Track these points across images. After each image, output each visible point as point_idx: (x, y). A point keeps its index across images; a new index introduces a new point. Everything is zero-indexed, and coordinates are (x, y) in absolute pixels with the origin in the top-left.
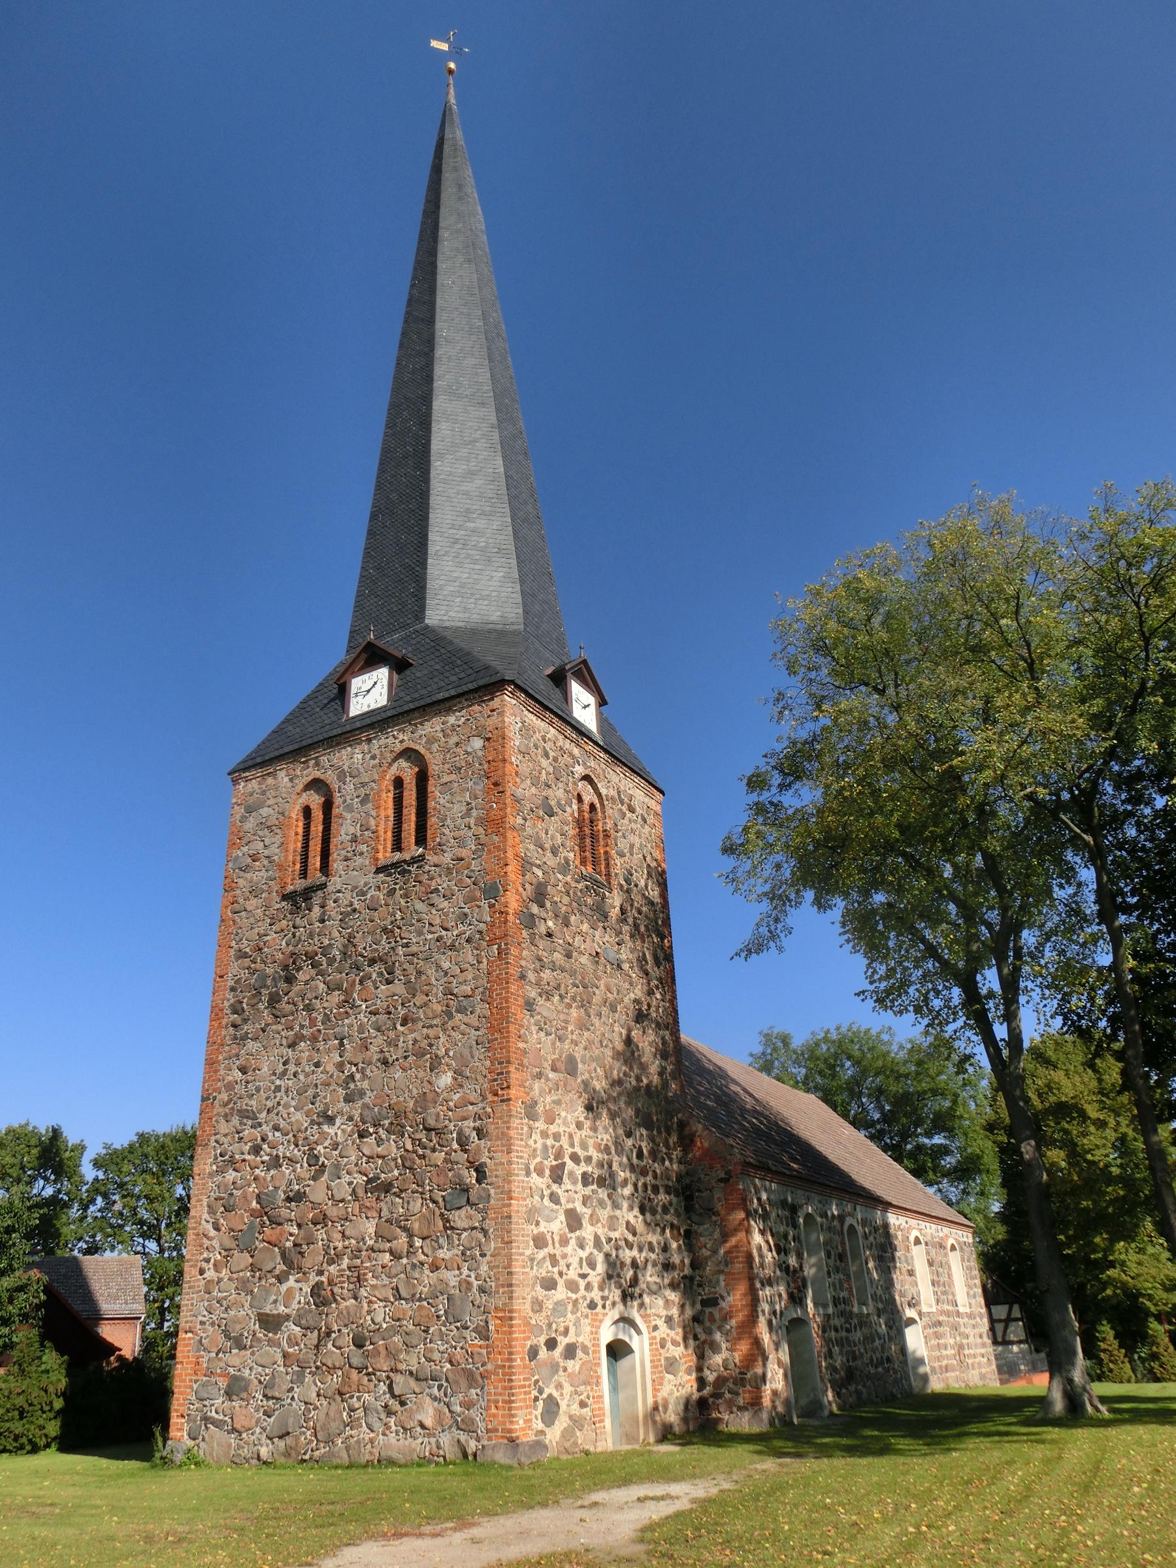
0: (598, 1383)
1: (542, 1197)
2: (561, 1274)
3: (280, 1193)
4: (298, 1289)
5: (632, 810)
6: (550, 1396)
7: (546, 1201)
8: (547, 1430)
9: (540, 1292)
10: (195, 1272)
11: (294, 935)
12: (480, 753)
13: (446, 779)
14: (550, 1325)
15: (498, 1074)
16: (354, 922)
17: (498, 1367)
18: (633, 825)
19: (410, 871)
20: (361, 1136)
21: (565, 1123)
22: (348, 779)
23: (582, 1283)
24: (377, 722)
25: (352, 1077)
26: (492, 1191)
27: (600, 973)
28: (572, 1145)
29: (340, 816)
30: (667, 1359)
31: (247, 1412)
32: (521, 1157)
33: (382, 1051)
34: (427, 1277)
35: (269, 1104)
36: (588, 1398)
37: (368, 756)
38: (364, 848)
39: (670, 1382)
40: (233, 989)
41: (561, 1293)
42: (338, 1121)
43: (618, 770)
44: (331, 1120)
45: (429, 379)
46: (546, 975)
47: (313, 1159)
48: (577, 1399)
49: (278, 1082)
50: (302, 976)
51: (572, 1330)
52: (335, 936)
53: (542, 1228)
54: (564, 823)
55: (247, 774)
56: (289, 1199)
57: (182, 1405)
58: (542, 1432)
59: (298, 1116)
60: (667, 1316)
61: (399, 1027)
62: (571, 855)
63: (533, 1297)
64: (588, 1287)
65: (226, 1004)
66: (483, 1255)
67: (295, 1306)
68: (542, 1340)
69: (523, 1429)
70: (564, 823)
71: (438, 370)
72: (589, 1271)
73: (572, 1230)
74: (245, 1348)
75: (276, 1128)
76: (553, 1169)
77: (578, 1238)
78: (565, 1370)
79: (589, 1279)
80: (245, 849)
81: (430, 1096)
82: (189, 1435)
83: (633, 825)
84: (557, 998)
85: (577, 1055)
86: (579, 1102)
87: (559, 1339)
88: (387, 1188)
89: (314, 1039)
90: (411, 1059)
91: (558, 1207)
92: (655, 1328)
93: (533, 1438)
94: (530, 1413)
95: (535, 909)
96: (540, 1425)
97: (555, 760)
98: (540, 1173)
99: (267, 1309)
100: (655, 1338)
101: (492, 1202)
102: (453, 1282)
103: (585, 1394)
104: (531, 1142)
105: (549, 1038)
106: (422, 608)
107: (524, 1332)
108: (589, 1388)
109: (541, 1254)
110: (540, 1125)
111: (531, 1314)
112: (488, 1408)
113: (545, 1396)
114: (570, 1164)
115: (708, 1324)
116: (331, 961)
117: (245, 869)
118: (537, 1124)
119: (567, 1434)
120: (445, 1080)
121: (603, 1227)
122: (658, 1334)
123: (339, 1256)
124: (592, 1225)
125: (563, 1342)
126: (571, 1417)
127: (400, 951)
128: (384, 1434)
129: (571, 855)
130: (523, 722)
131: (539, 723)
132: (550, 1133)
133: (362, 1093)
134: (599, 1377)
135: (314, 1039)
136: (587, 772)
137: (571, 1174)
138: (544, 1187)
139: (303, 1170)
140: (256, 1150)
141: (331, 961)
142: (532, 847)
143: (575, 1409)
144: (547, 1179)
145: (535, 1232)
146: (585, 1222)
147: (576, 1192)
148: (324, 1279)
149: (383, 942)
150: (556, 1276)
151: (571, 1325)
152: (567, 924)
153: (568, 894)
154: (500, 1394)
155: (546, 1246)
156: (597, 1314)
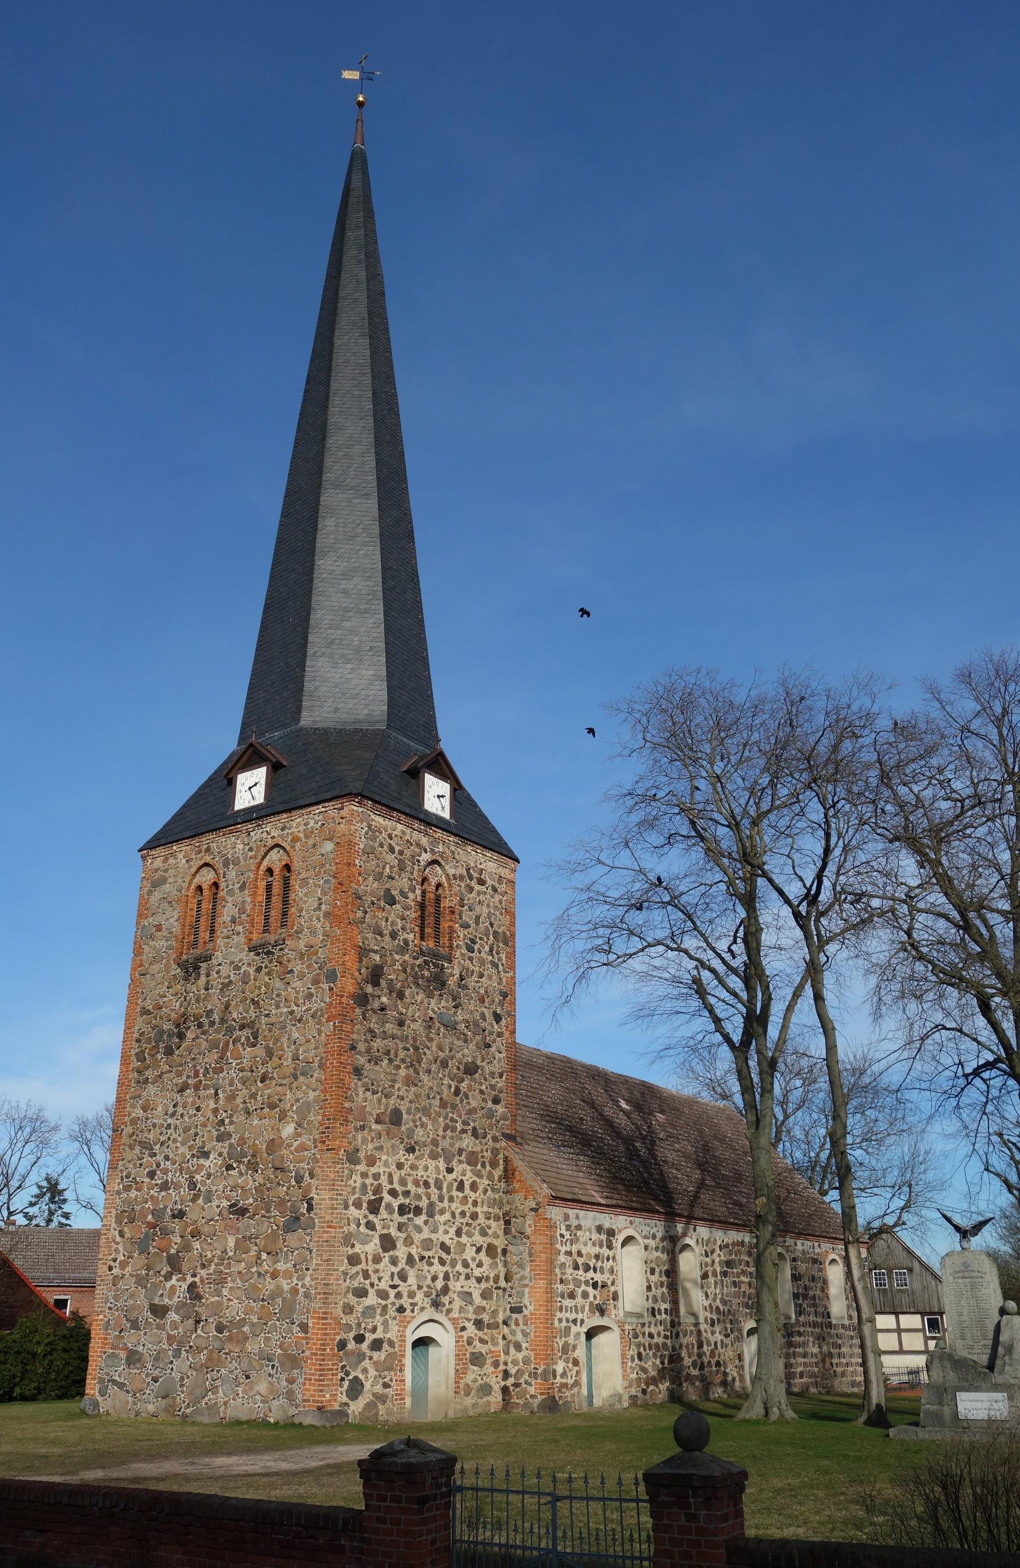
0: (401, 1370)
1: (359, 1225)
2: (372, 1285)
3: (168, 1210)
4: (179, 1285)
5: (481, 882)
6: (356, 1378)
7: (363, 1229)
8: (351, 1403)
9: (352, 1300)
10: (105, 1268)
11: (185, 998)
12: (331, 856)
13: (303, 875)
14: (359, 1325)
15: (327, 1128)
16: (233, 992)
17: (312, 1354)
18: (482, 897)
19: (273, 953)
20: (227, 1169)
21: (386, 1164)
22: (231, 866)
23: (392, 1293)
24: (255, 815)
25: (222, 1121)
26: (316, 1221)
27: (432, 1036)
28: (391, 1182)
29: (223, 899)
30: (473, 1354)
31: (138, 1376)
32: (341, 1195)
33: (245, 1102)
34: (270, 1284)
35: (162, 1138)
36: (391, 1380)
37: (247, 847)
38: (240, 929)
39: (474, 1372)
40: (138, 1041)
41: (372, 1299)
42: (212, 1157)
43: (469, 849)
44: (206, 1155)
45: (319, 473)
46: (378, 1044)
47: (192, 1185)
48: (381, 1381)
49: (170, 1121)
50: (190, 1035)
51: (380, 1329)
52: (215, 1004)
53: (358, 1249)
54: (407, 908)
55: (153, 852)
56: (174, 1216)
57: (95, 1370)
58: (346, 1404)
59: (183, 1150)
60: (476, 1320)
61: (259, 1083)
62: (411, 936)
63: (344, 1303)
64: (399, 1295)
65: (133, 1052)
66: (307, 1269)
67: (176, 1299)
68: (352, 1335)
69: (329, 1401)
70: (407, 908)
71: (328, 461)
72: (401, 1283)
73: (385, 1249)
74: (139, 1329)
75: (167, 1158)
76: (370, 1203)
77: (391, 1257)
78: (371, 1358)
79: (400, 1289)
80: (151, 920)
81: (277, 1142)
82: (99, 1392)
83: (482, 897)
84: (386, 1061)
85: (402, 1108)
86: (401, 1146)
87: (367, 1335)
88: (242, 1212)
89: (197, 1087)
90: (266, 1110)
91: (373, 1233)
92: (463, 1329)
93: (338, 1408)
94: (336, 1390)
95: (369, 989)
96: (345, 1399)
97: (401, 853)
98: (358, 1205)
99: (157, 1301)
100: (462, 1337)
101: (316, 1229)
102: (286, 1288)
103: (389, 1378)
104: (351, 1182)
105: (376, 1096)
106: (299, 710)
107: (335, 1329)
108: (392, 1373)
109: (354, 1270)
110: (362, 1167)
111: (342, 1315)
112: (304, 1384)
113: (351, 1377)
114: (387, 1198)
115: (513, 1327)
116: (212, 1024)
117: (152, 937)
118: (358, 1167)
119: (371, 1406)
120: (288, 1130)
121: (418, 1247)
122: (465, 1334)
123: (210, 1261)
124: (406, 1246)
125: (370, 1337)
126: (374, 1394)
127: (263, 1019)
128: (234, 1399)
129: (411, 936)
130: (369, 826)
131: (388, 823)
132: (370, 1174)
133: (229, 1135)
134: (404, 1365)
135: (197, 1087)
136: (434, 858)
137: (389, 1206)
138: (361, 1217)
139: (184, 1190)
140: (152, 1175)
141: (212, 1024)
142: (370, 936)
143: (379, 1389)
144: (365, 1210)
145: (350, 1253)
146: (399, 1244)
147: (392, 1220)
148: (197, 1279)
149: (250, 1012)
150: (368, 1287)
151: (379, 1324)
152: (401, 995)
153: (405, 971)
154: (313, 1374)
155: (361, 1263)
156: (405, 1317)
